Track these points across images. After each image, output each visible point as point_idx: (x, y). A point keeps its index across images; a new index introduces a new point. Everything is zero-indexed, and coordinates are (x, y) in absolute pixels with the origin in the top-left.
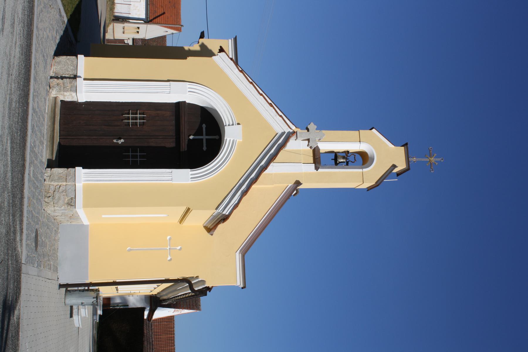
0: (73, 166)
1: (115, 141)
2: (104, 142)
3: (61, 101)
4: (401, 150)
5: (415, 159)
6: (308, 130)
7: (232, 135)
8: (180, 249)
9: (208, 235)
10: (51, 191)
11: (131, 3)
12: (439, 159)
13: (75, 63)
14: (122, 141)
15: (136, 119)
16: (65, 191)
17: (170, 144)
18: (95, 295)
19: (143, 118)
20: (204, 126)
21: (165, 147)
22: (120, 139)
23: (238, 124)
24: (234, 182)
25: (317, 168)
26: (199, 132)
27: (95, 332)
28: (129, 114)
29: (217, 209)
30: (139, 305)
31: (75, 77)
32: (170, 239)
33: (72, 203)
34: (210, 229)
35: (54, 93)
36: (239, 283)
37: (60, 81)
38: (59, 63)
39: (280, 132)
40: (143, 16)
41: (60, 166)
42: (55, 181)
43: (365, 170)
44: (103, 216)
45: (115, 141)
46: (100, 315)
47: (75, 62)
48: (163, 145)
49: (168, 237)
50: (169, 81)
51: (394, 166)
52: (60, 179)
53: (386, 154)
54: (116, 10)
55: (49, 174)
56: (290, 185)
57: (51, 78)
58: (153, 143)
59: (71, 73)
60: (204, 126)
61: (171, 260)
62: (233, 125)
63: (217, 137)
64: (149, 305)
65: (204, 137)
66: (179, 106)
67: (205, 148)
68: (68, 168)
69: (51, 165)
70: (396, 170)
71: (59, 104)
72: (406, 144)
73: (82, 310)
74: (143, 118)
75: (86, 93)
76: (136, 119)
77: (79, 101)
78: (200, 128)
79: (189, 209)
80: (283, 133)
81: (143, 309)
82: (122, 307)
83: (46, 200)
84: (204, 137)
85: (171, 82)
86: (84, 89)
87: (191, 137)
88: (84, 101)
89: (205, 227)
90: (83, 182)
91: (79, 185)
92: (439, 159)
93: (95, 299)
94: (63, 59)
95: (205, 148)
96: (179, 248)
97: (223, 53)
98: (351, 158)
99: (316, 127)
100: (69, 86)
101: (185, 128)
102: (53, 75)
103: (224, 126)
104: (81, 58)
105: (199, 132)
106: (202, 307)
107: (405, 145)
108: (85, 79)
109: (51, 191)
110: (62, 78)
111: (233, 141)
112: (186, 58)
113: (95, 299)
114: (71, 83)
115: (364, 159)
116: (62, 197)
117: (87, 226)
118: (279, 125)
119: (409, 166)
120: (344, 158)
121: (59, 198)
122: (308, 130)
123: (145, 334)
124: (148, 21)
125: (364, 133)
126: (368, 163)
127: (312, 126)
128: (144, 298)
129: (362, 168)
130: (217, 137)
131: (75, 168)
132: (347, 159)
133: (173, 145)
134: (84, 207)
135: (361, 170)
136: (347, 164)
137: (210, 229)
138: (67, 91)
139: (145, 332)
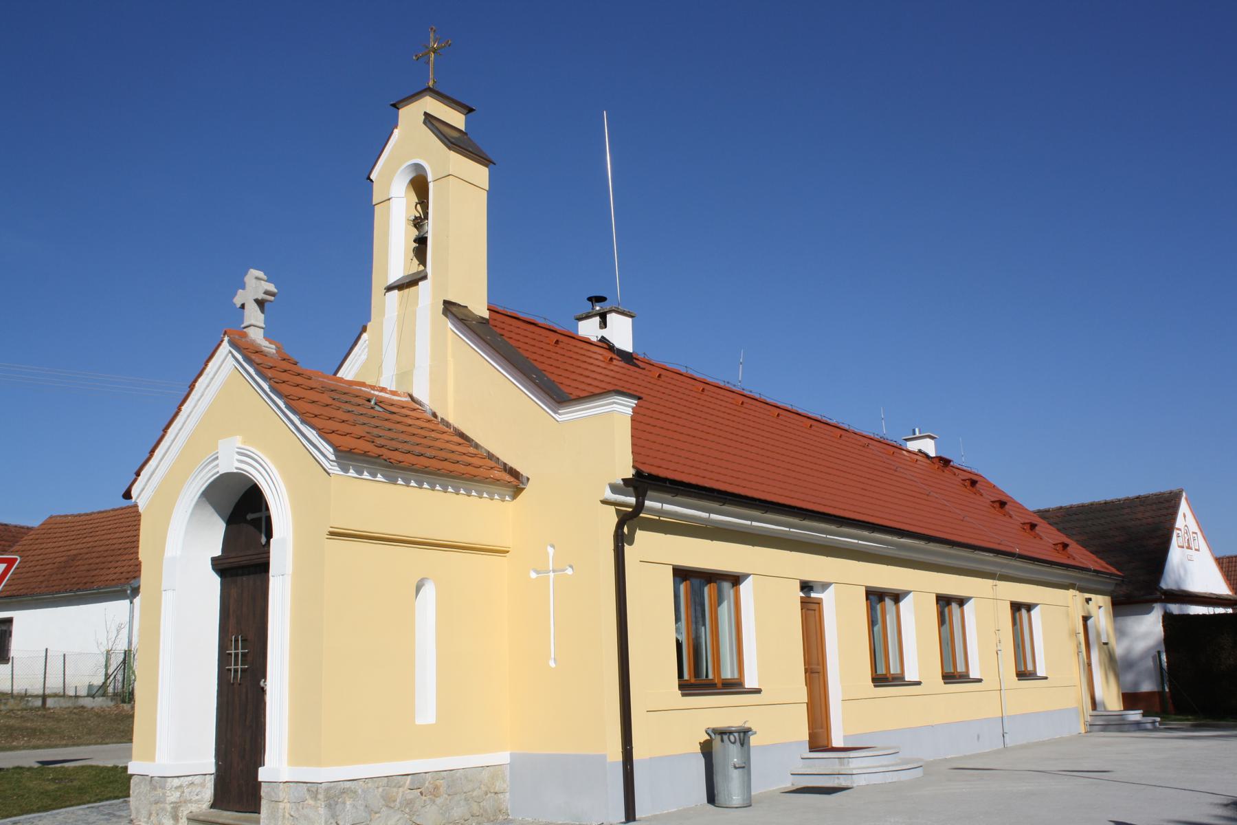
0: (257, 786)
3: (212, 806)
6: (243, 306)
8: (553, 546)
18: (718, 737)
20: (250, 517)
34: (514, 482)
36: (633, 402)
43: (430, 179)
44: (426, 714)
46: (1144, 715)
49: (533, 575)
51: (429, 119)
53: (411, 141)
56: (450, 325)
68: (259, 798)
70: (457, 119)
72: (394, 105)
73: (851, 766)
74: (236, 641)
77: (213, 769)
79: (332, 534)
88: (212, 760)
89: (514, 497)
93: (725, 737)
96: (551, 550)
97: (134, 493)
99: (240, 291)
106: (1174, 487)
107: (396, 106)
111: (239, 453)
113: (725, 737)
122: (243, 306)
127: (238, 301)
135: (431, 186)
137: (514, 482)
138: (164, 794)
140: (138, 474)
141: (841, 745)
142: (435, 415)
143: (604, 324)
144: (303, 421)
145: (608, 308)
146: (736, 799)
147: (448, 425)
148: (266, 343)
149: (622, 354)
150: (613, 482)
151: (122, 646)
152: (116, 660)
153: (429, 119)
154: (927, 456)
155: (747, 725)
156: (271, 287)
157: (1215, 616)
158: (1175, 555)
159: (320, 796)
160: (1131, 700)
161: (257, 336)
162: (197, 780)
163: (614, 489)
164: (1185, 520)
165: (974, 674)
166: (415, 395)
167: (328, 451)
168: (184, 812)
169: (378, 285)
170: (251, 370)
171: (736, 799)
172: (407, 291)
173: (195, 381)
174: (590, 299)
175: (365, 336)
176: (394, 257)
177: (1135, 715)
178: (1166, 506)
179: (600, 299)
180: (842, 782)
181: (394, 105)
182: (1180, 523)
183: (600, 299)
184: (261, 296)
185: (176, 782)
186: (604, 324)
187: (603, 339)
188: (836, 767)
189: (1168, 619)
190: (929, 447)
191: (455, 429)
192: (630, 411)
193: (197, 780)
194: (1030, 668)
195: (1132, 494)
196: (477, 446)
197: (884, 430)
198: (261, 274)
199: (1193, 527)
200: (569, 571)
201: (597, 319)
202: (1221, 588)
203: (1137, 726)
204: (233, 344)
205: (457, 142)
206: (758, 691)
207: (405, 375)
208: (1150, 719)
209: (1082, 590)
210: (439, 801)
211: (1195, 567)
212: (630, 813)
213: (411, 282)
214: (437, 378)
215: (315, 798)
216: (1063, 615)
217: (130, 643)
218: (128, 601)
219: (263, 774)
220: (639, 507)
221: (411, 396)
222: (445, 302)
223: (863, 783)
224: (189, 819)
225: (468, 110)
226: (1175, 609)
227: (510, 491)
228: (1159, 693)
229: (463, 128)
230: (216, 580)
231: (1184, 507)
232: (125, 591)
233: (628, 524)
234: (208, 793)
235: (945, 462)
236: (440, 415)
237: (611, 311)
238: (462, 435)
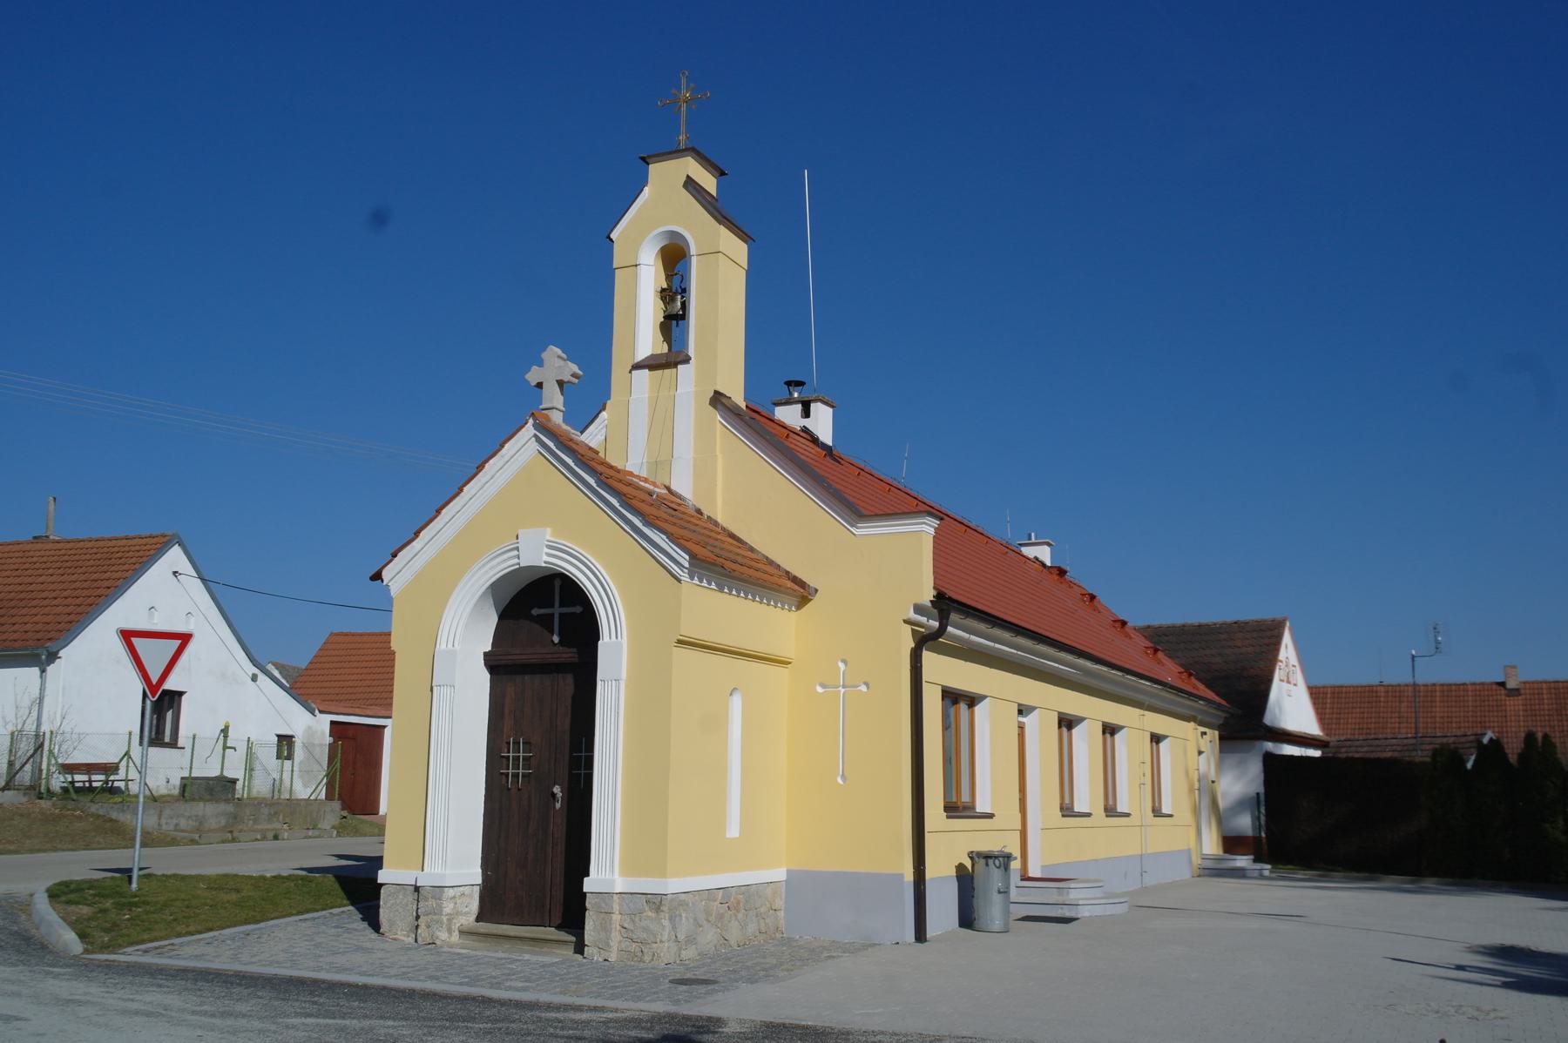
1: (558, 806)
3: (478, 919)
4: (655, 169)
6: (540, 385)
7: (538, 550)
8: (844, 661)
9: (817, 599)
12: (684, 81)
13: (392, 889)
14: (557, 789)
15: (517, 759)
18: (982, 861)
19: (517, 743)
20: (535, 612)
21: (573, 698)
22: (554, 795)
25: (687, 360)
27: (1429, 883)
29: (679, 581)
30: (1255, 769)
32: (823, 686)
33: (655, 902)
34: (799, 593)
35: (448, 937)
38: (392, 923)
39: (536, 446)
41: (582, 927)
42: (608, 938)
43: (693, 251)
44: (733, 831)
45: (558, 806)
46: (1255, 861)
47: (392, 889)
48: (569, 701)
49: (820, 690)
51: (690, 184)
52: (605, 928)
55: (595, 951)
59: (411, 897)
60: (535, 612)
61: (866, 684)
62: (517, 549)
64: (1258, 743)
65: (557, 610)
66: (493, 663)
68: (585, 909)
69: (580, 948)
70: (709, 182)
71: (485, 927)
72: (643, 159)
74: (517, 743)
76: (517, 759)
77: (479, 881)
79: (679, 642)
81: (1270, 761)
82: (1263, 810)
83: (647, 958)
84: (557, 610)
86: (438, 870)
87: (556, 639)
89: (799, 608)
90: (616, 876)
92: (684, 81)
93: (990, 861)
96: (841, 665)
97: (386, 574)
99: (535, 368)
100: (432, 903)
103: (522, 569)
105: (546, 622)
106: (1278, 616)
107: (645, 161)
112: (394, 653)
114: (426, 900)
115: (674, 257)
116: (644, 923)
117: (789, 872)
118: (523, 447)
119: (686, 150)
120: (673, 300)
121: (646, 929)
122: (540, 385)
123: (1396, 754)
126: (681, 243)
127: (533, 376)
128: (1232, 759)
130: (557, 583)
132: (676, 293)
133: (570, 679)
134: (663, 874)
135: (694, 260)
137: (799, 593)
138: (440, 907)
139: (1389, 755)
140: (394, 555)
141: (1039, 875)
142: (699, 512)
143: (806, 413)
144: (648, 523)
145: (814, 396)
146: (997, 924)
147: (716, 524)
148: (565, 427)
149: (824, 446)
150: (919, 601)
151: (30, 727)
152: (25, 747)
153: (690, 184)
154: (1043, 565)
155: (1007, 850)
156: (575, 368)
157: (1301, 758)
158: (1277, 690)
159: (665, 908)
160: (1232, 844)
161: (557, 418)
162: (467, 890)
163: (919, 609)
164: (1287, 651)
165: (981, 806)
166: (673, 487)
167: (684, 559)
168: (456, 926)
169: (620, 362)
170: (569, 461)
171: (997, 924)
172: (660, 372)
173: (487, 461)
174: (788, 383)
175: (604, 414)
176: (641, 331)
177: (1243, 861)
178: (1266, 636)
179: (800, 384)
180: (1067, 913)
181: (643, 159)
182: (1282, 655)
183: (800, 384)
184: (567, 377)
185: (451, 892)
186: (806, 413)
187: (805, 430)
188: (1054, 897)
189: (1270, 761)
190: (1044, 554)
191: (724, 529)
192: (932, 531)
193: (467, 890)
194: (965, 798)
195: (1230, 618)
196: (752, 549)
197: (1008, 535)
198: (559, 351)
199: (1293, 660)
200: (864, 688)
201: (799, 406)
202: (1312, 727)
203: (1239, 873)
204: (537, 426)
205: (717, 209)
206: (991, 816)
207: (662, 462)
208: (1259, 866)
209: (1201, 724)
210: (740, 916)
211: (1292, 706)
212: (920, 935)
213: (670, 360)
214: (703, 472)
215: (658, 909)
216: (1189, 747)
217: (39, 725)
218: (36, 670)
219: (589, 885)
220: (941, 631)
221: (668, 488)
222: (716, 392)
223: (1087, 914)
224: (461, 932)
225: (720, 173)
226: (1270, 746)
227: (795, 600)
228: (1254, 838)
229: (714, 193)
230: (485, 677)
231: (1287, 639)
232: (38, 656)
233: (924, 641)
234: (474, 905)
235: (1062, 572)
236: (706, 512)
237: (816, 401)
238: (732, 536)
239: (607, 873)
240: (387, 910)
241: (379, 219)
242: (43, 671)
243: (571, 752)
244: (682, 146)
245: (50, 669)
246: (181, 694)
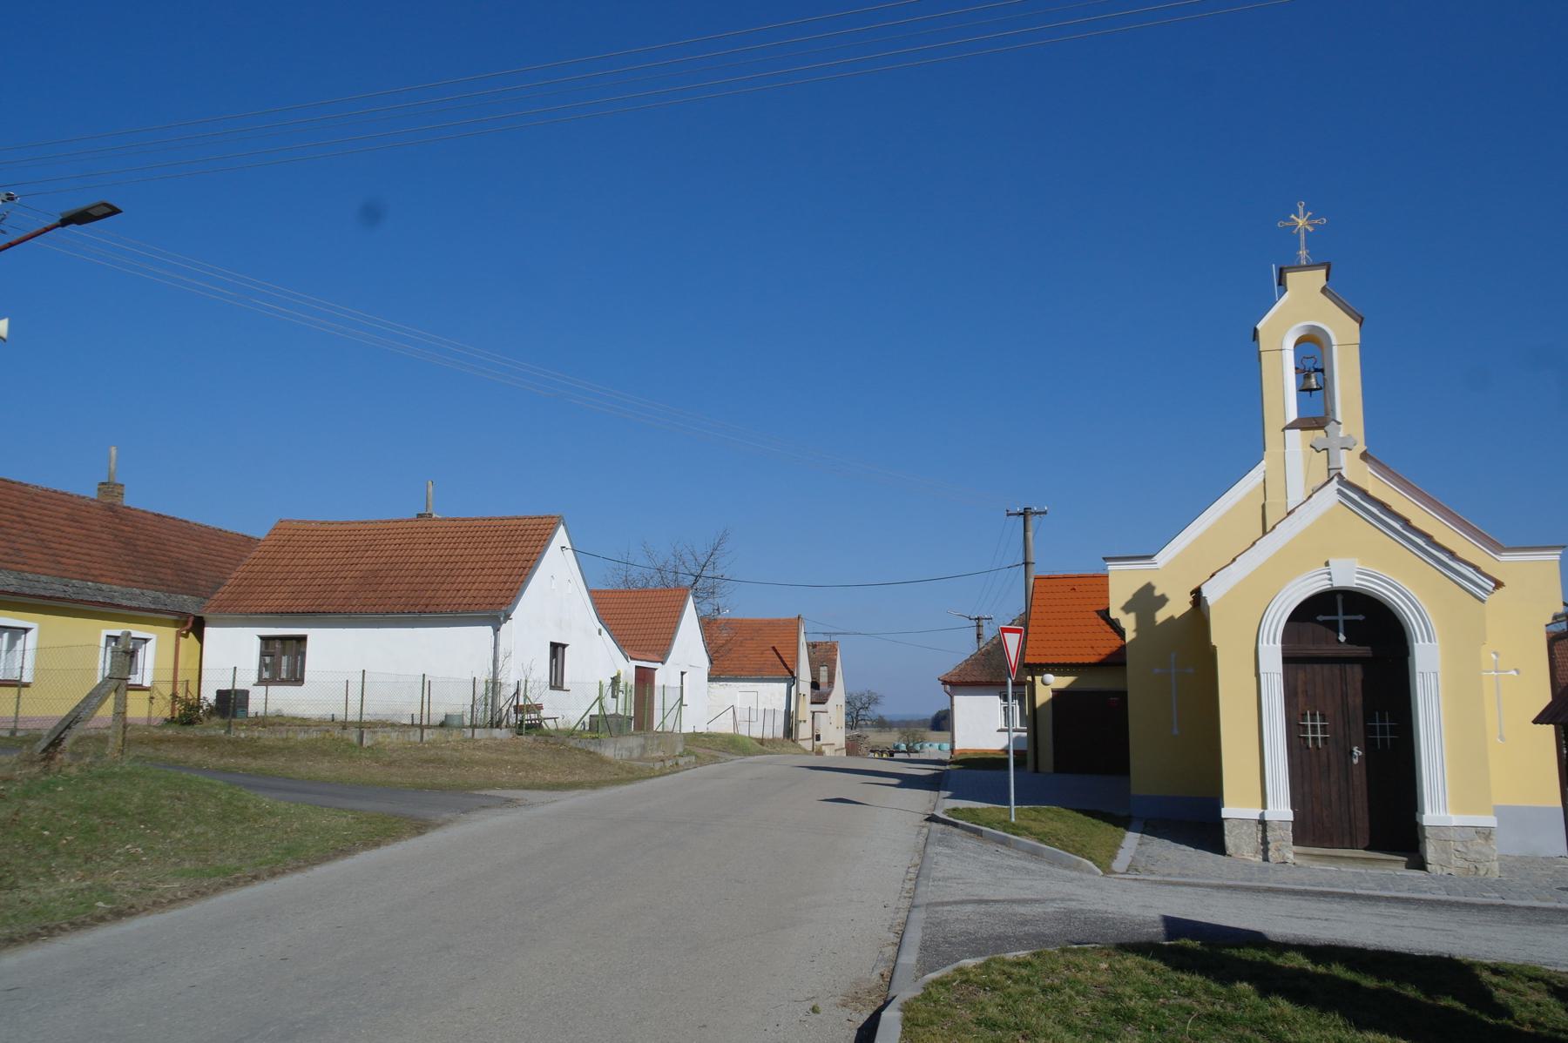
1: (1356, 761)
2: (1359, 780)
5: (1303, 253)
7: (1347, 575)
10: (1466, 864)
11: (761, 708)
15: (1314, 727)
16: (1464, 843)
17: (1356, 673)
20: (1320, 618)
23: (1327, 564)
24: (1431, 574)
26: (1333, 626)
28: (1306, 739)
31: (1263, 823)
37: (1271, 846)
38: (1238, 847)
39: (1338, 497)
40: (784, 686)
43: (1334, 341)
45: (1356, 761)
48: (1359, 685)
50: (1258, 675)
53: (1301, 306)
54: (768, 734)
57: (1266, 859)
58: (1356, 700)
60: (1320, 618)
63: (1339, 598)
66: (1287, 660)
67: (1361, 617)
69: (1419, 863)
75: (1281, 810)
76: (1383, 728)
78: (1324, 623)
80: (1339, 492)
83: (1482, 873)
85: (1262, 670)
87: (1342, 638)
91: (1456, 820)
94: (1229, 841)
95: (1361, 617)
98: (1309, 364)
101: (1327, 650)
102: (1259, 858)
104: (1226, 812)
105: (1333, 626)
108: (1264, 806)
109: (1466, 864)
110: (1265, 842)
120: (1307, 377)
121: (1479, 853)
124: (791, 678)
125: (1264, 343)
129: (1331, 345)
130: (1339, 598)
131: (1423, 827)
135: (1335, 349)
136: (1322, 371)
239: (1438, 809)
240: (1431, 852)
241: (371, 214)
242: (496, 630)
243: (1365, 721)
244: (1304, 262)
245: (504, 627)
246: (564, 646)
